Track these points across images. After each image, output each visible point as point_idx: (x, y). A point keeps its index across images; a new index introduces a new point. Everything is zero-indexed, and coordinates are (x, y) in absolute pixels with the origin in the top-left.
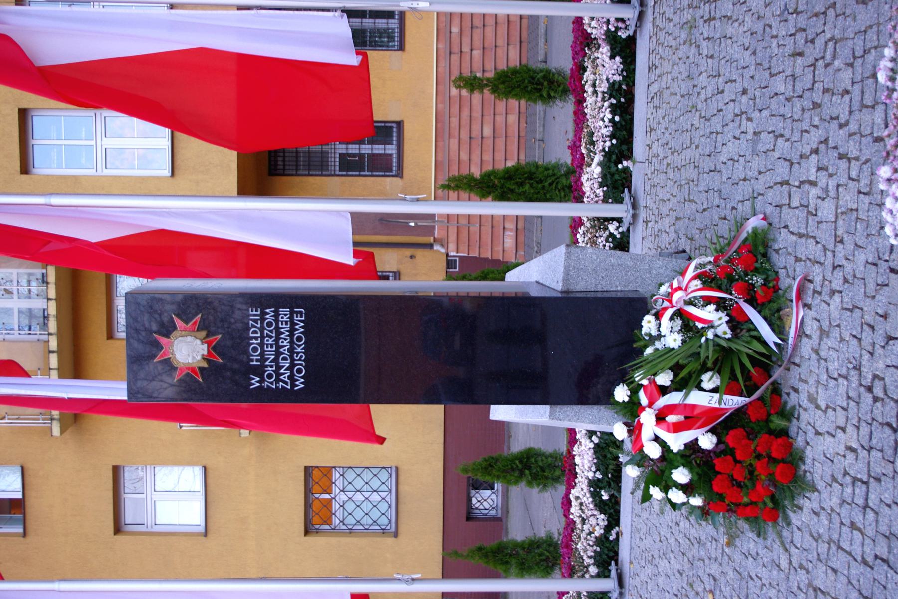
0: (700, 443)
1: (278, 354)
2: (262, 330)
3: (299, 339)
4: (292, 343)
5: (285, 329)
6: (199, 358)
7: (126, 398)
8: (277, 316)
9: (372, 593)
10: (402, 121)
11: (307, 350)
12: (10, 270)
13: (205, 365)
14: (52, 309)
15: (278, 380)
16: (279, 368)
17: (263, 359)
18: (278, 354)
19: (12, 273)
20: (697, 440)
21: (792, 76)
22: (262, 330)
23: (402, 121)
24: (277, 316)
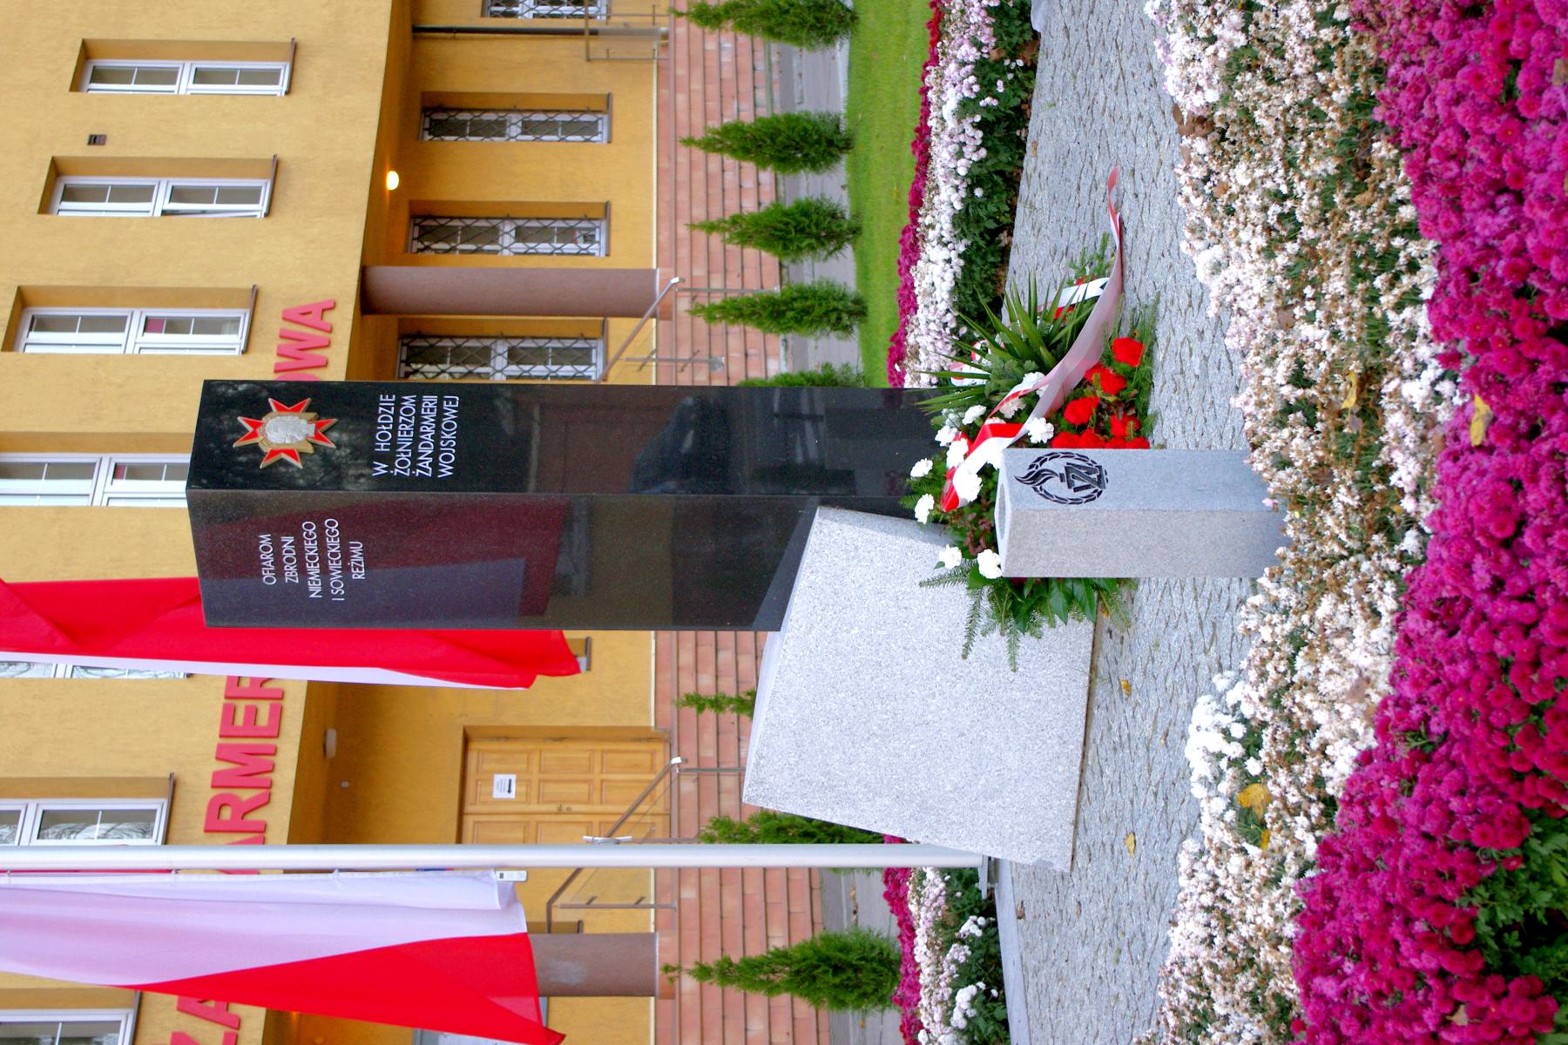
0: (988, 552)
1: (417, 440)
2: (396, 415)
3: (449, 425)
4: (438, 429)
5: (430, 417)
6: (301, 438)
7: (187, 567)
8: (418, 404)
9: (478, 728)
10: (209, 387)
11: (458, 438)
12: (542, 497)
13: (310, 450)
14: (593, 373)
15: (414, 467)
16: (416, 454)
17: (394, 444)
18: (417, 440)
19: (538, 490)
20: (996, 551)
21: (691, 290)
22: (396, 415)
23: (209, 387)
24: (418, 404)
